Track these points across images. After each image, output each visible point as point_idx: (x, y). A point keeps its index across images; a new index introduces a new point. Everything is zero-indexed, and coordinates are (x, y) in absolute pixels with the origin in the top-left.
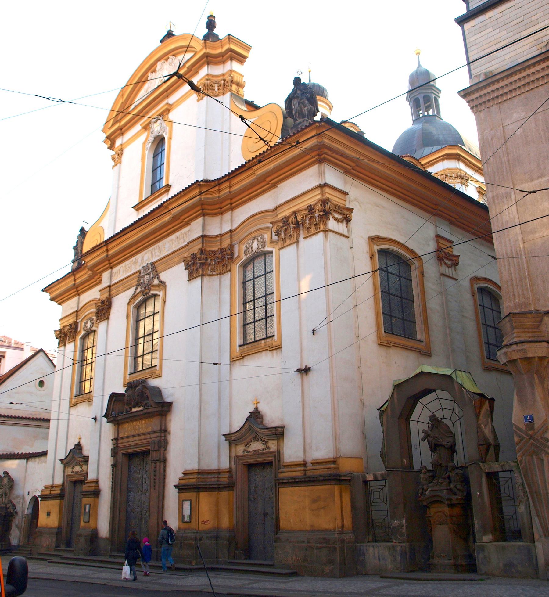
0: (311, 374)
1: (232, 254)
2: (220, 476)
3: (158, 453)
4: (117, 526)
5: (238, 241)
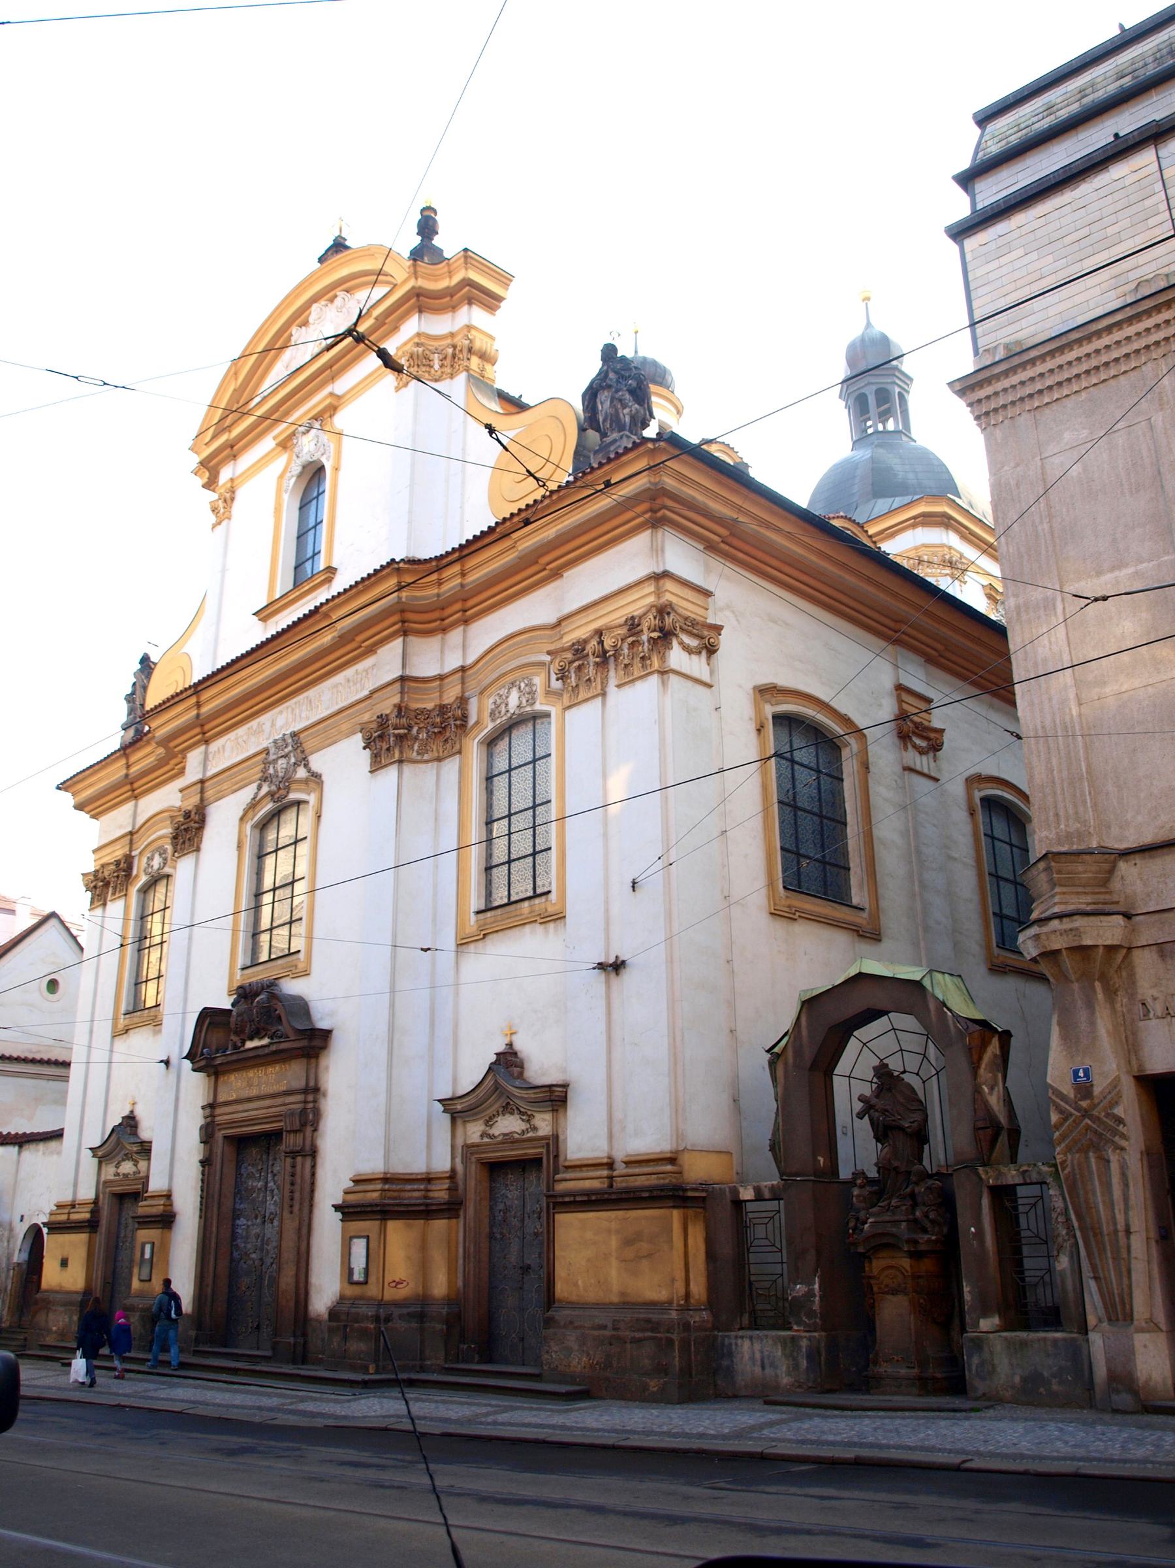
0: (627, 975)
1: (465, 717)
2: (430, 1187)
3: (300, 1137)
4: (209, 1290)
5: (478, 690)
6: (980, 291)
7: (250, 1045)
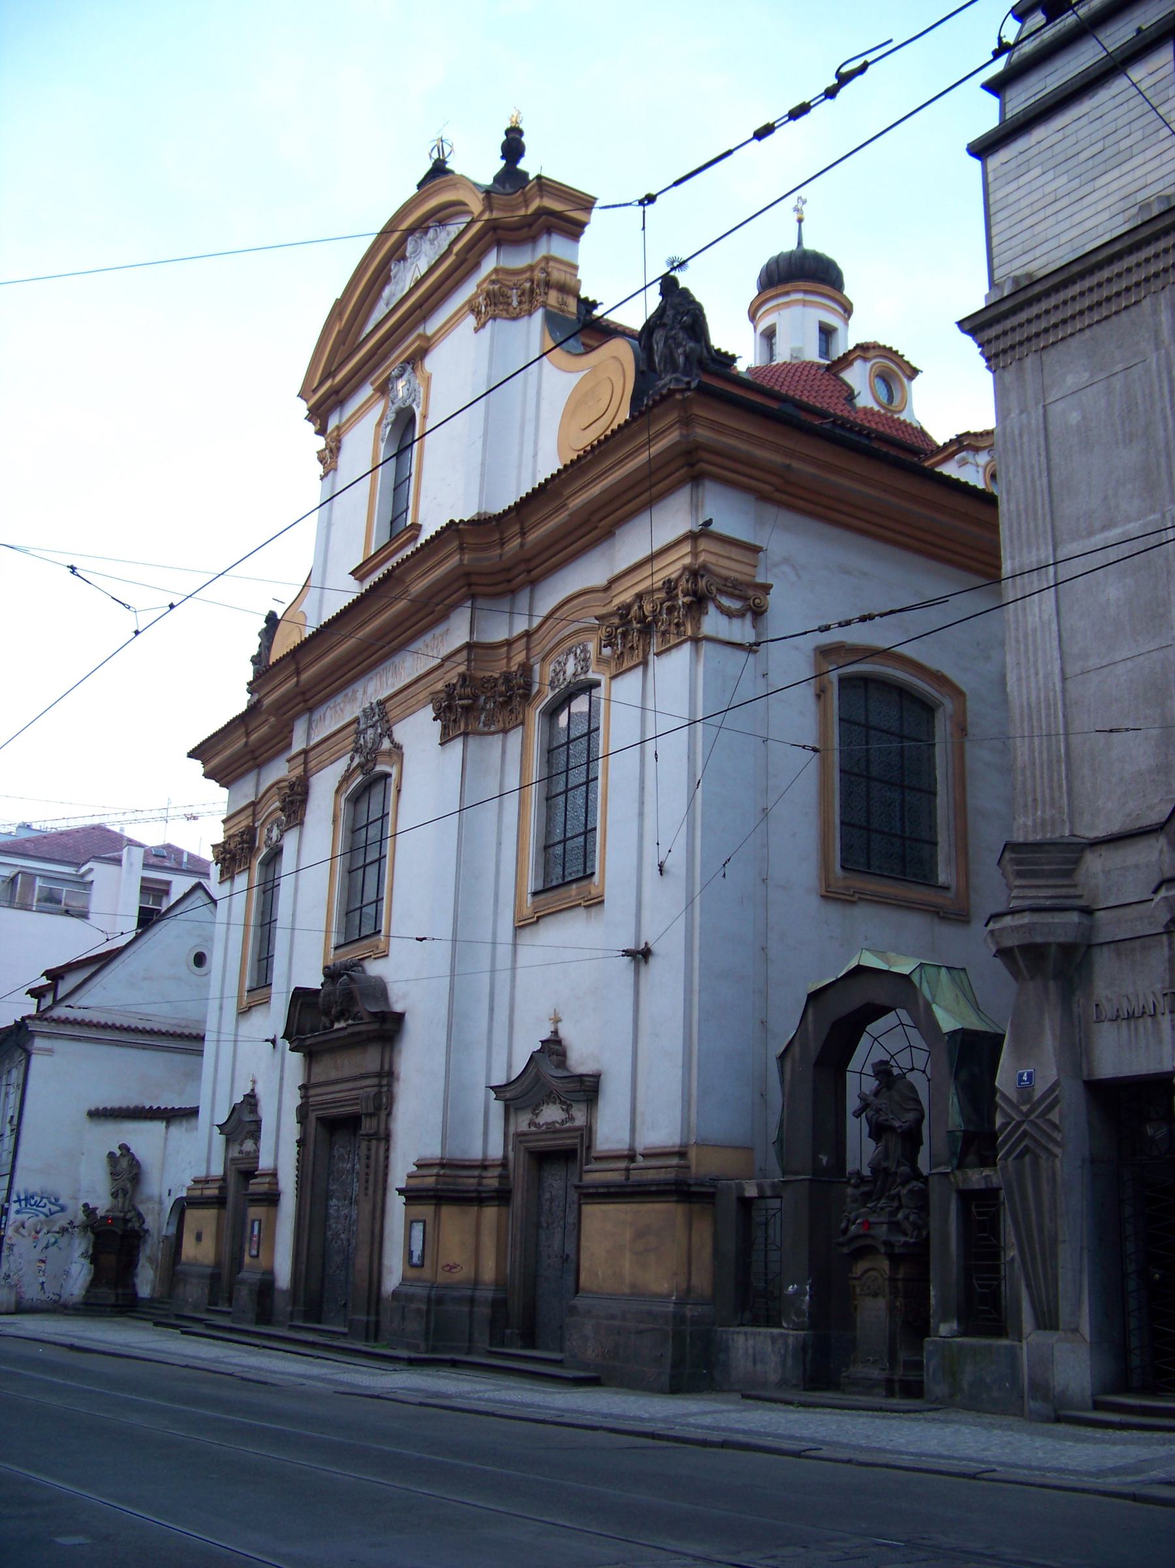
1: (528, 685)
2: (485, 1174)
3: (375, 1120)
4: (303, 1267)
5: (541, 656)
6: (1000, 216)
7: (337, 1026)
